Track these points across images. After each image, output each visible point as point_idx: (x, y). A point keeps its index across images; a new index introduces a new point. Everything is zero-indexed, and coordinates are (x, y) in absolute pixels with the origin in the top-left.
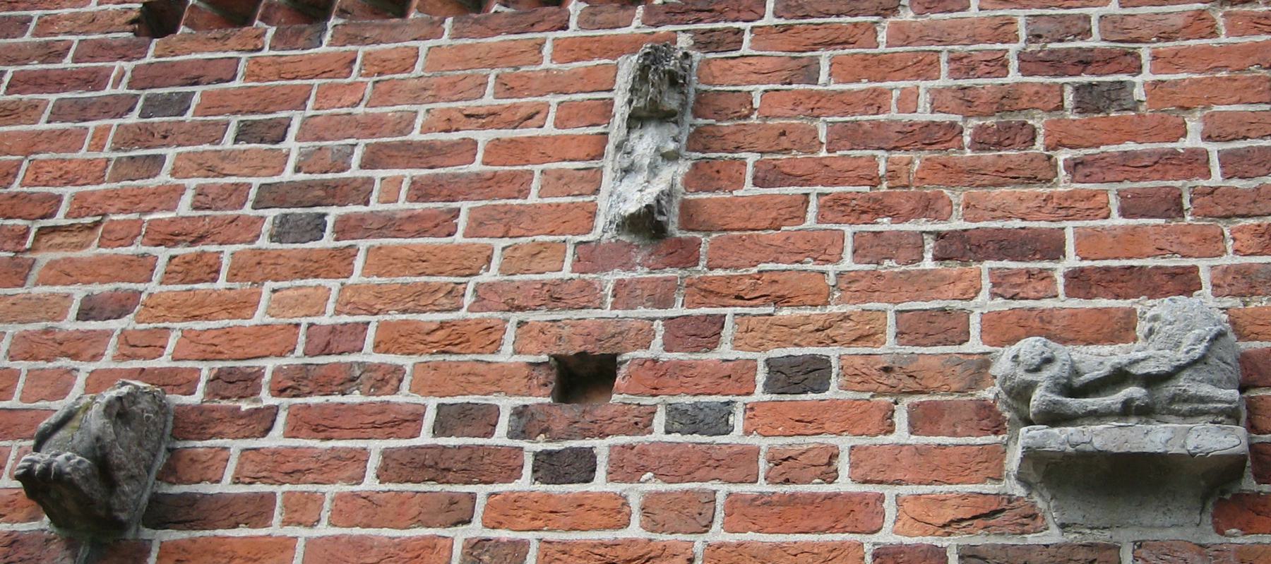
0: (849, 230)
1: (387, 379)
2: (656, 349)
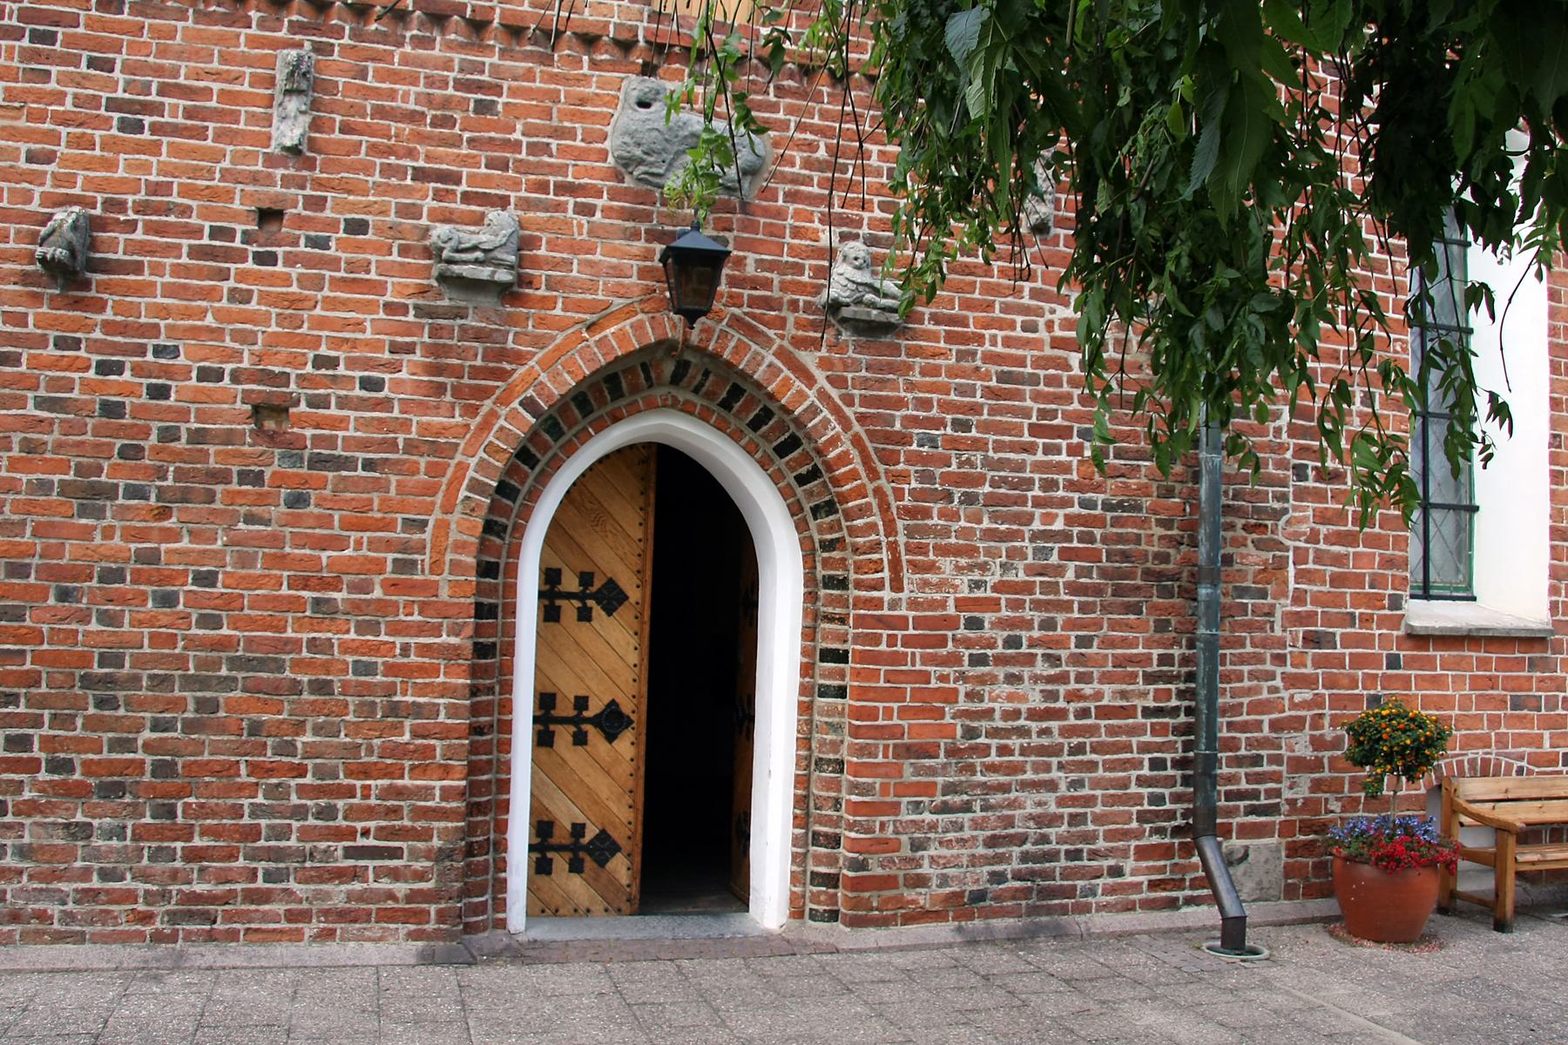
0: (378, 161)
1: (185, 211)
2: (300, 209)
